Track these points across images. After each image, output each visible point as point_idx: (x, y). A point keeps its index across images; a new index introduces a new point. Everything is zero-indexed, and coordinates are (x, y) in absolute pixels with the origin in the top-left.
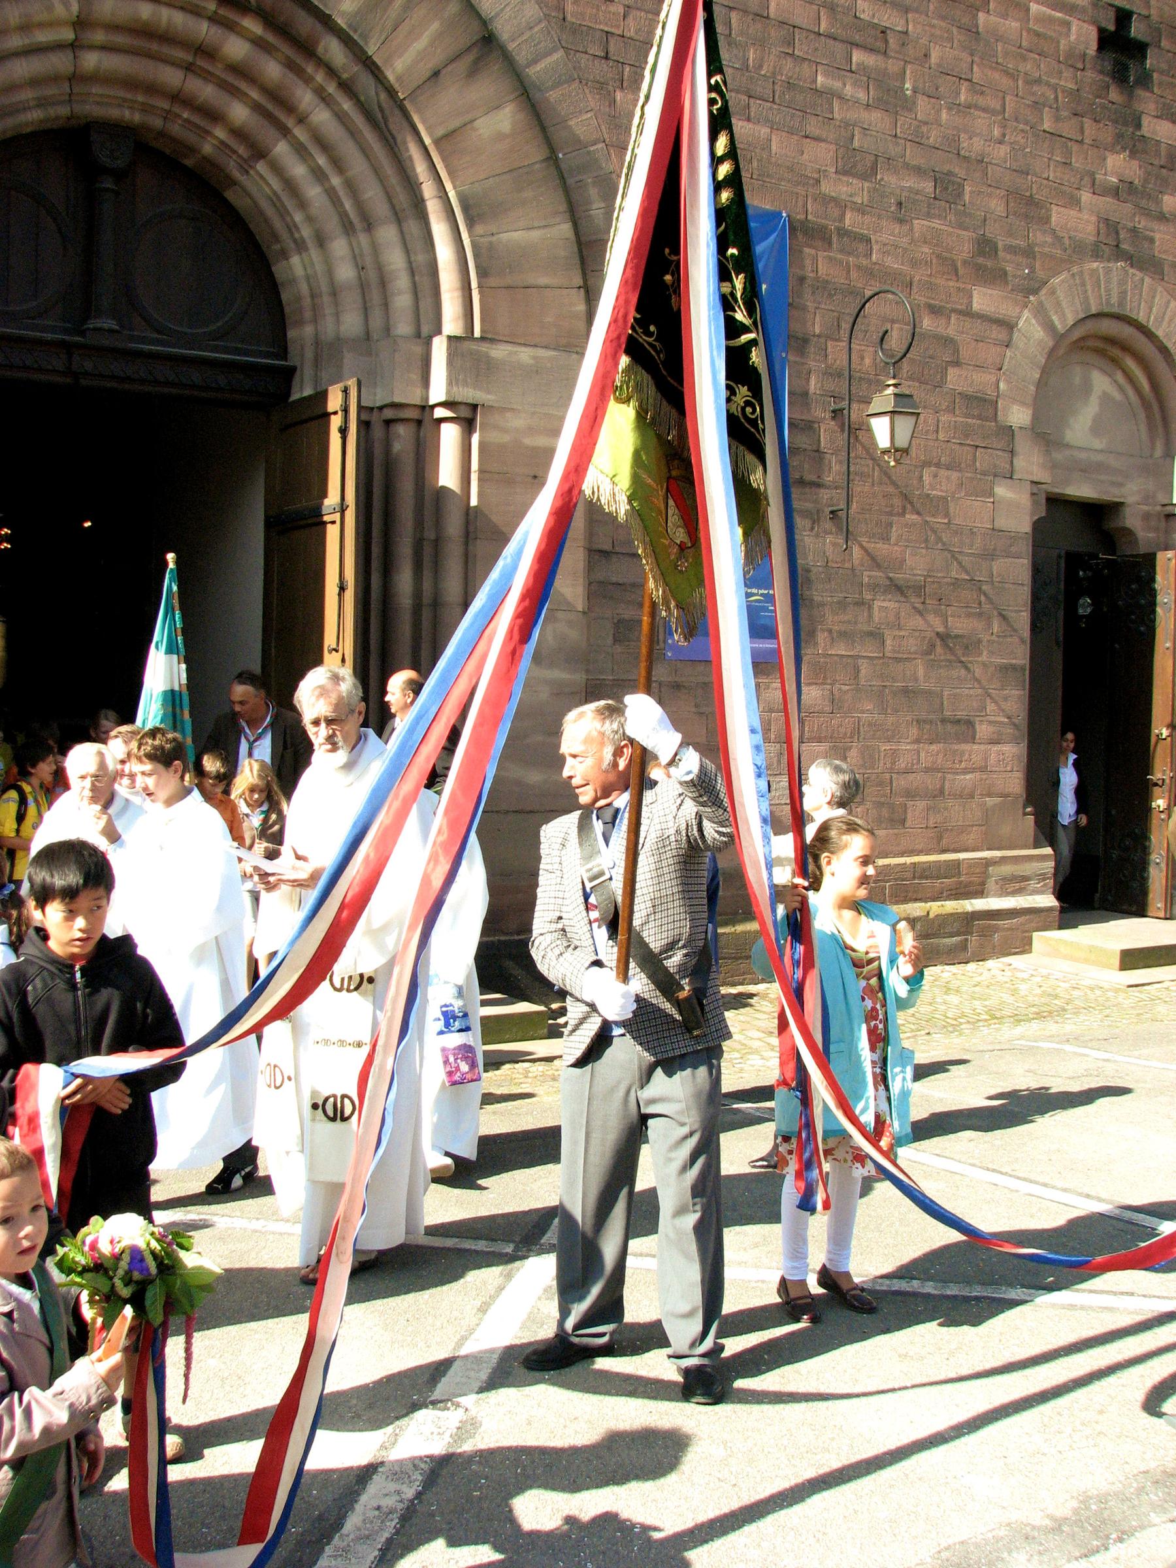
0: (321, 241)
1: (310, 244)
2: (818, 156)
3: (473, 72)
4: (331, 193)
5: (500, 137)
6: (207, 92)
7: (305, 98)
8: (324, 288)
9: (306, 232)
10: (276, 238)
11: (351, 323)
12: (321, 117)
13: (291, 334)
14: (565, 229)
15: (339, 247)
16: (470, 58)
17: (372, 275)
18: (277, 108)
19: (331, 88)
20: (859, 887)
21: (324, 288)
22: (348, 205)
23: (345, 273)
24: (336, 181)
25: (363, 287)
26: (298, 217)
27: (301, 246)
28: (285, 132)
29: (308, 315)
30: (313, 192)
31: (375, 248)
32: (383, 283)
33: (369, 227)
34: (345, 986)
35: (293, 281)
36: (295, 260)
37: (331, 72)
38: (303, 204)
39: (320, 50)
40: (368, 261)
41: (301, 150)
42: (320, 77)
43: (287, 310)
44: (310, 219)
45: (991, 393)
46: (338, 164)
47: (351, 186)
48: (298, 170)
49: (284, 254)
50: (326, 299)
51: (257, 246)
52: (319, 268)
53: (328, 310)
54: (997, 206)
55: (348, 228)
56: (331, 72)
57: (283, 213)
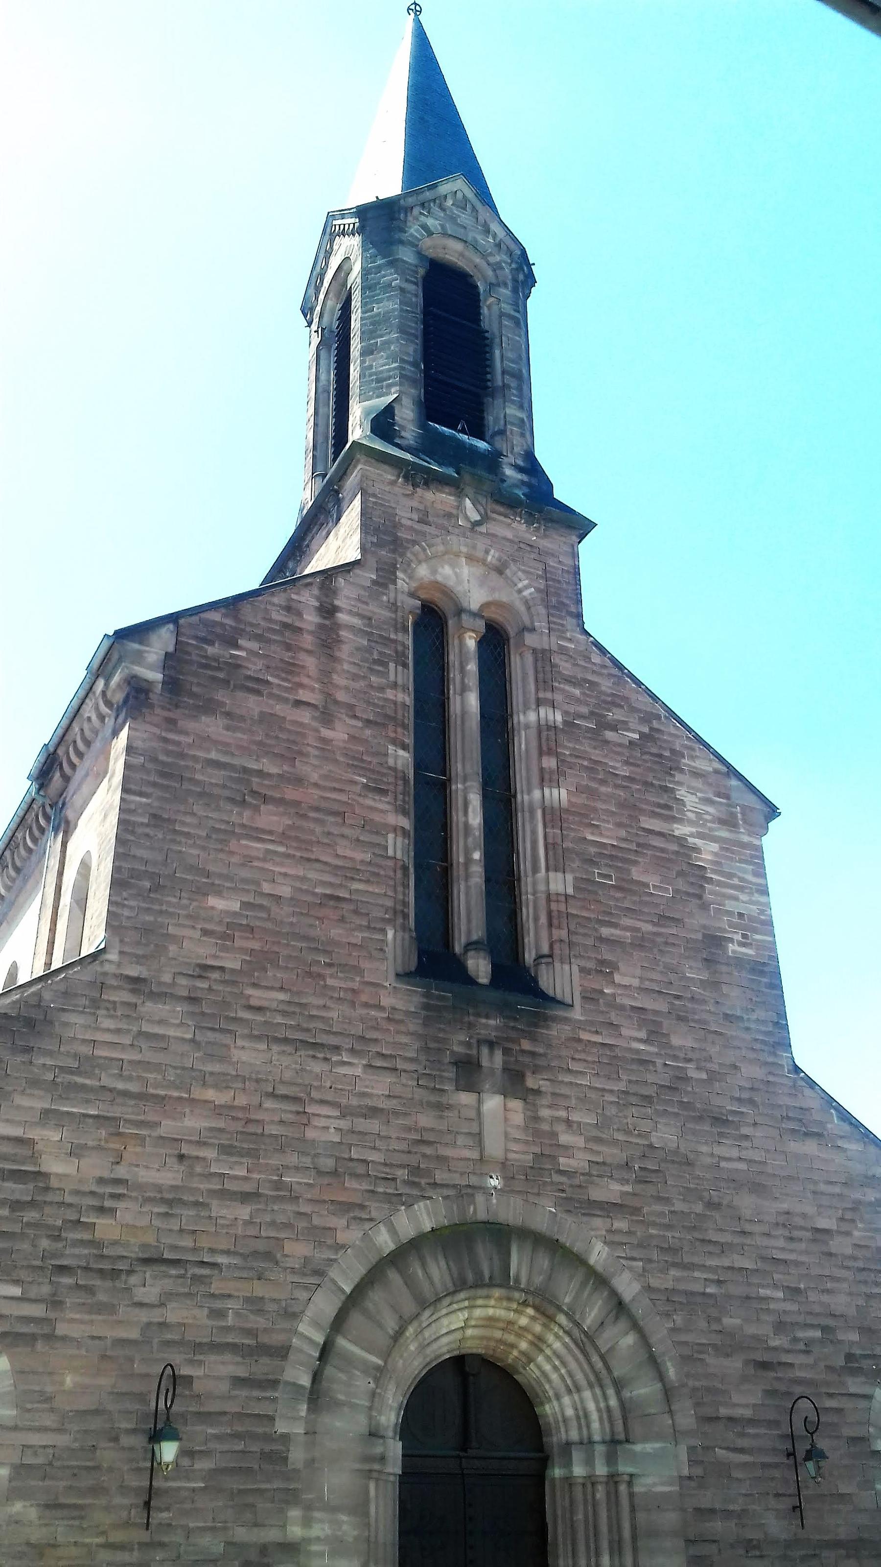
0: (558, 1397)
1: (553, 1399)
2: (764, 1330)
3: (617, 1318)
4: (562, 1377)
5: (629, 1346)
6: (511, 1338)
7: (551, 1338)
8: (560, 1419)
9: (551, 1393)
10: (537, 1396)
11: (574, 1435)
12: (557, 1345)
13: (544, 1439)
14: (659, 1385)
15: (566, 1400)
16: (614, 1312)
17: (581, 1413)
18: (538, 1343)
19: (561, 1333)
20: (374, 1368)
21: (560, 1419)
22: (569, 1382)
23: (570, 1412)
24: (563, 1371)
25: (578, 1417)
26: (547, 1387)
27: (549, 1400)
28: (541, 1351)
29: (554, 1432)
30: (554, 1376)
31: (582, 1401)
32: (586, 1415)
33: (578, 1390)
34: (545, 748)
35: (546, 1416)
36: (547, 1407)
37: (560, 1326)
38: (549, 1381)
39: (563, 1400)
40: (579, 1407)
41: (548, 1359)
42: (556, 1329)
43: (542, 1428)
44: (552, 1387)
45: (866, 1435)
46: (564, 1364)
47: (571, 1375)
48: (547, 1367)
49: (542, 1404)
50: (561, 1424)
51: (530, 1402)
52: (557, 1409)
53: (563, 1429)
54: (854, 1337)
55: (569, 1392)
56: (560, 1326)
57: (541, 1385)
